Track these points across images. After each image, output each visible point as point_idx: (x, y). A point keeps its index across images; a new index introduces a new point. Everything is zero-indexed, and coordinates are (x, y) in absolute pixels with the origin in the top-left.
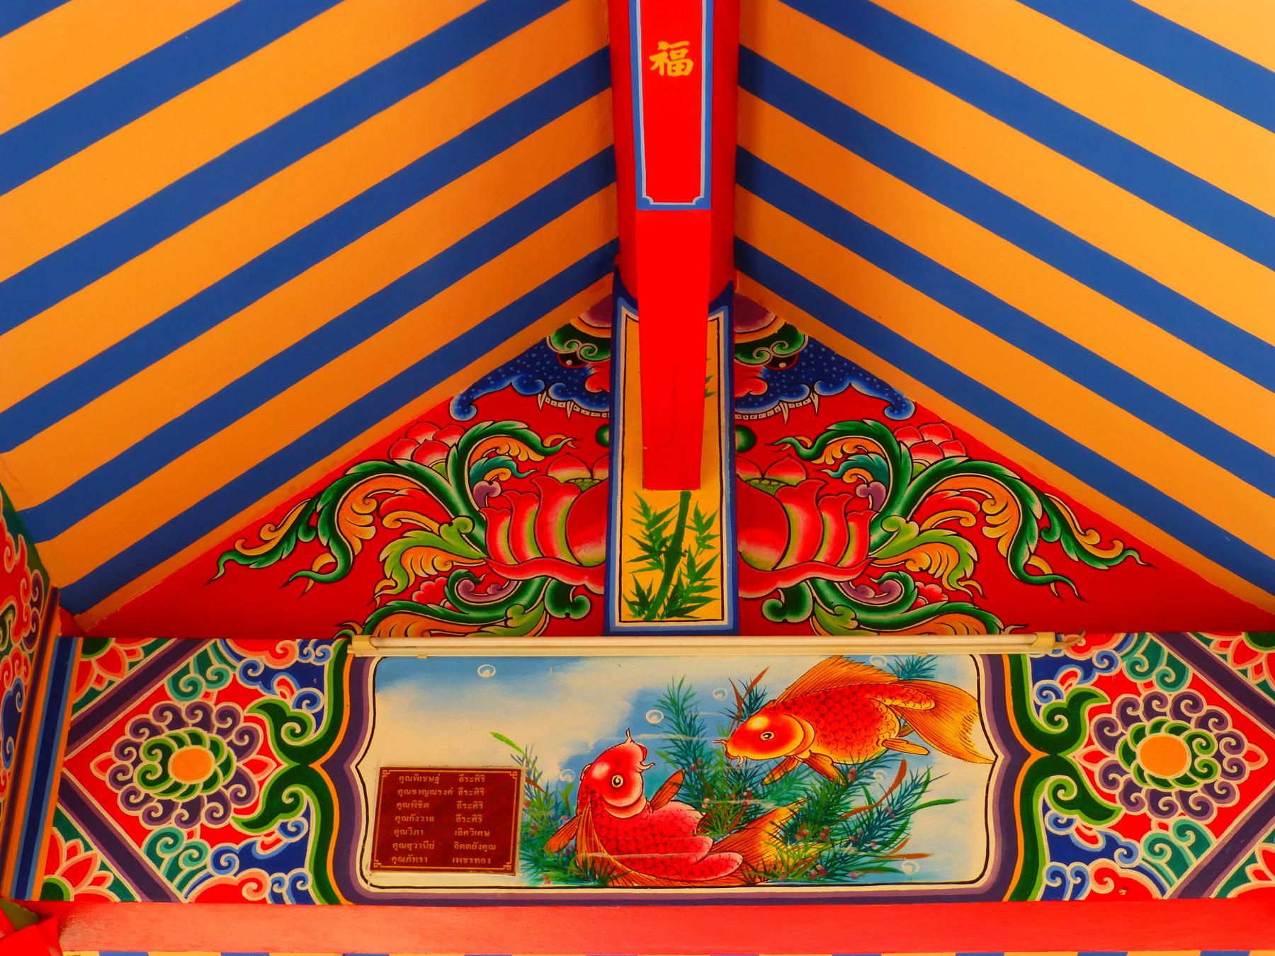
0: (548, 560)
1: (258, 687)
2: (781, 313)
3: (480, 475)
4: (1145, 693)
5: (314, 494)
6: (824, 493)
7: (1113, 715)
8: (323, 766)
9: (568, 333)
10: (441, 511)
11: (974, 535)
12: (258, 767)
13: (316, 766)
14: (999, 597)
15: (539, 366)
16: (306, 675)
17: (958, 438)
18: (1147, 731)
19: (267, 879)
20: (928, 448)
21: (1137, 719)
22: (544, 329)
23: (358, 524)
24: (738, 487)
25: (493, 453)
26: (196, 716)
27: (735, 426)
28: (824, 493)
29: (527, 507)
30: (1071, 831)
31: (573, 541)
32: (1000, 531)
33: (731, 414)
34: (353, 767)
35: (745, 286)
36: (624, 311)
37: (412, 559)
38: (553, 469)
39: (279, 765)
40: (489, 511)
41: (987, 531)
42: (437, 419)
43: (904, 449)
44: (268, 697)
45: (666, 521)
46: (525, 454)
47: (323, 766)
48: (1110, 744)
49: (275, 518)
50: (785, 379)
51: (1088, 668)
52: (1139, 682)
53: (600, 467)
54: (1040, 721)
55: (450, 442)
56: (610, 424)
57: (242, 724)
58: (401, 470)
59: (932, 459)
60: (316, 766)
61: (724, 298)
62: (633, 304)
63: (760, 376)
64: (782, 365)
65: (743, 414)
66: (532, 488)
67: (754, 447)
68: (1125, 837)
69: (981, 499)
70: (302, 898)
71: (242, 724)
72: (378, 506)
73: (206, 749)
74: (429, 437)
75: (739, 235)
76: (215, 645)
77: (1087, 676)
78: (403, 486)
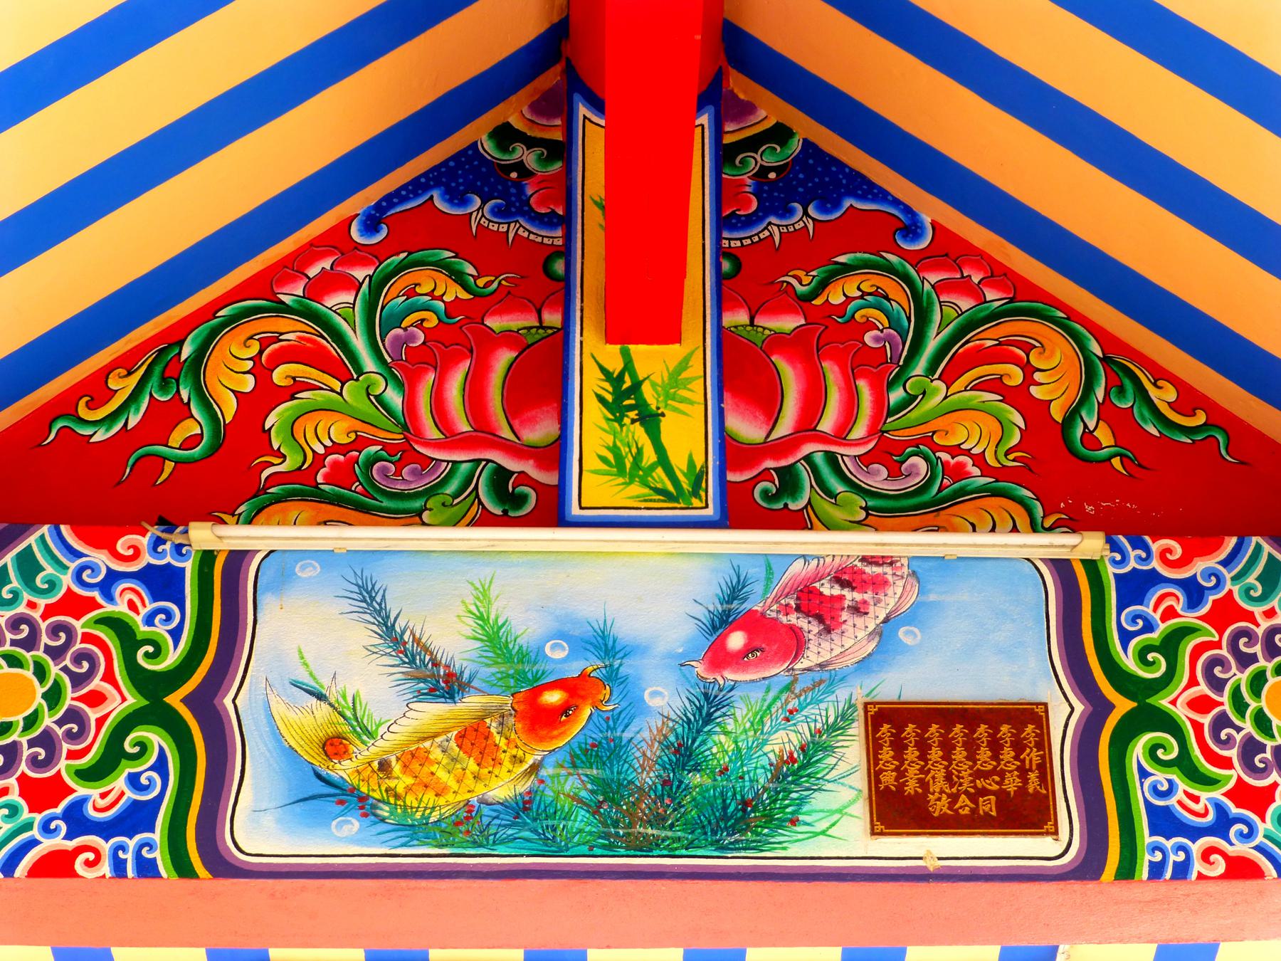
0: (483, 435)
1: (96, 594)
2: (770, 110)
3: (396, 319)
4: (1265, 624)
5: (175, 336)
6: (829, 336)
7: (1224, 652)
8: (185, 701)
9: (505, 135)
10: (345, 369)
11: (1018, 397)
12: (96, 699)
13: (174, 700)
14: (1051, 478)
15: (465, 175)
16: (163, 583)
17: (999, 274)
18: (1269, 674)
19: (105, 847)
20: (964, 287)
21: (1253, 659)
22: (478, 133)
23: (230, 378)
24: (724, 339)
25: (411, 293)
26: (19, 631)
27: (720, 253)
28: (829, 336)
29: (457, 363)
30: (1172, 802)
31: (516, 407)
32: (1054, 391)
33: (718, 239)
34: (228, 702)
35: (740, 86)
36: (583, 110)
37: (310, 427)
38: (494, 314)
39: (124, 699)
40: (406, 368)
41: (1034, 390)
42: (336, 240)
43: (927, 287)
44: (108, 609)
45: (656, 395)
46: (454, 292)
47: (185, 701)
48: (1218, 685)
49: (126, 363)
50: (777, 194)
51: (1194, 592)
52: (1258, 610)
53: (553, 308)
54: (1129, 662)
55: (360, 274)
56: (566, 252)
57: (78, 646)
58: (288, 309)
59: (965, 304)
60: (174, 700)
61: (714, 97)
62: (598, 105)
63: (748, 189)
64: (772, 175)
65: (733, 240)
66: (459, 338)
67: (739, 281)
68: (1238, 806)
69: (1028, 348)
70: (147, 869)
71: (78, 646)
72: (261, 352)
73: (29, 673)
74: (326, 264)
75: (727, 16)
76: (42, 537)
77: (1194, 603)
78: (292, 331)
